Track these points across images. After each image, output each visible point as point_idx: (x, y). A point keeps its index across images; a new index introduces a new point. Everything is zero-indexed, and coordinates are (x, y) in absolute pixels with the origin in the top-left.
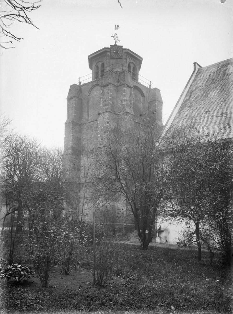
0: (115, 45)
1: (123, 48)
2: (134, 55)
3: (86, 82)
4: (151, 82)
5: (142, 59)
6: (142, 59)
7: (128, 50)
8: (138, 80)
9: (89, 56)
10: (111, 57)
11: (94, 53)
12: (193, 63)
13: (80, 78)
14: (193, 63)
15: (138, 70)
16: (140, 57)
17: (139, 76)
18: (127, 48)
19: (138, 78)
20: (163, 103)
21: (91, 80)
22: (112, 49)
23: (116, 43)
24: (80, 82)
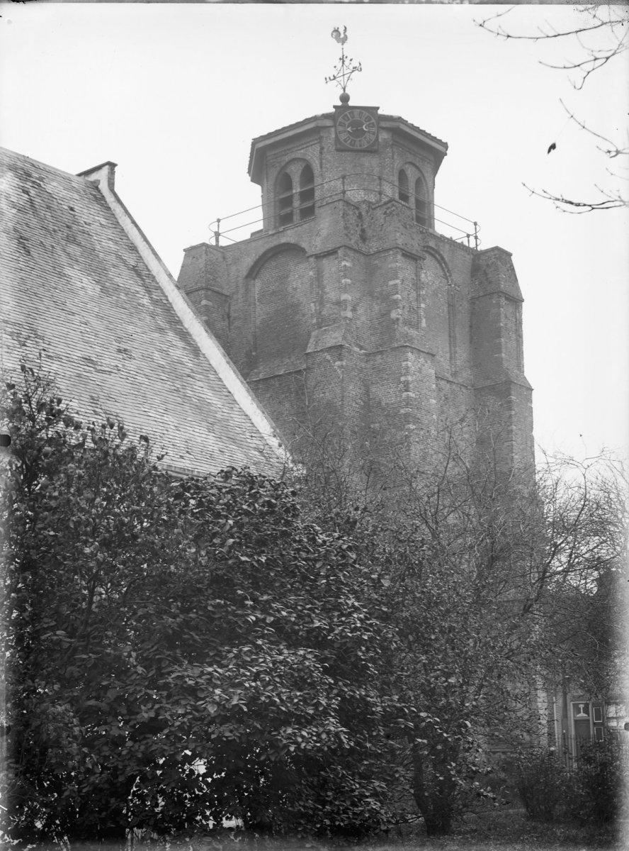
0: (344, 107)
1: (380, 112)
2: (420, 137)
3: (245, 235)
4: (475, 224)
5: (445, 145)
6: (447, 147)
7: (400, 119)
8: (431, 225)
9: (255, 142)
10: (339, 146)
11: (265, 133)
12: (184, 250)
13: (219, 221)
14: (184, 250)
15: (430, 184)
16: (439, 142)
17: (436, 209)
18: (436, 186)
19: (431, 217)
20: (522, 301)
21: (260, 226)
22: (340, 119)
23: (344, 89)
24: (217, 235)
